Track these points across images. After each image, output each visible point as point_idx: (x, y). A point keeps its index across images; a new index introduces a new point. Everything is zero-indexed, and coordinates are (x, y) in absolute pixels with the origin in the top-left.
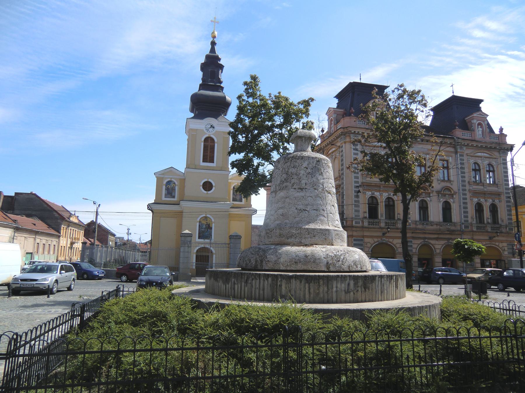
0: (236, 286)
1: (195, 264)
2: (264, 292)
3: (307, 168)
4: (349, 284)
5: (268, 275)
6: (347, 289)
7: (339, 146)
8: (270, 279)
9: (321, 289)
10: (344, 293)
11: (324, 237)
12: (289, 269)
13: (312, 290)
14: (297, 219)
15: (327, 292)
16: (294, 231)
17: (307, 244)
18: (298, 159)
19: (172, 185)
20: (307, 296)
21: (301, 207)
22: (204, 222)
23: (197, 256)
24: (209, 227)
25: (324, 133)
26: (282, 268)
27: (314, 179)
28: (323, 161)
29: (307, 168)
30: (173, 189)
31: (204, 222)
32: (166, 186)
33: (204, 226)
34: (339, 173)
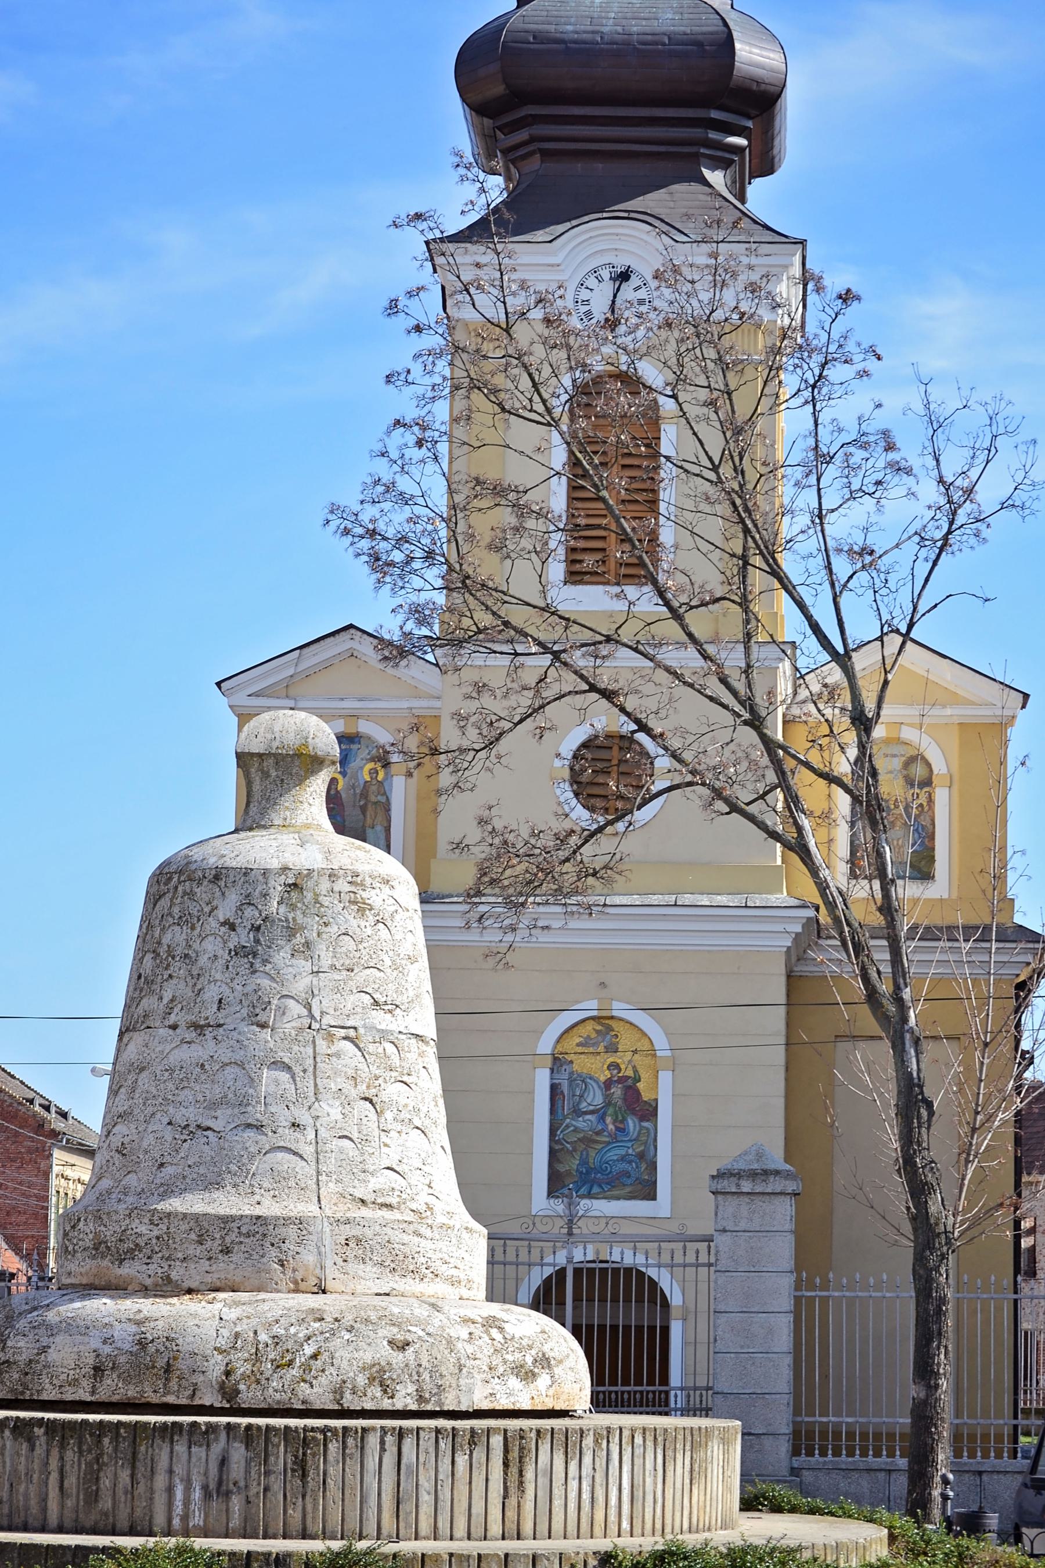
4: (223, 1462)
5: (64, 1424)
12: (68, 1397)
13: (71, 1481)
14: (169, 1170)
15: (131, 1492)
16: (143, 1229)
17: (194, 1285)
20: (53, 1506)
21: (191, 1114)
22: (594, 1066)
26: (50, 1394)
28: (325, 885)
29: (232, 927)
31: (594, 1066)
33: (595, 1098)
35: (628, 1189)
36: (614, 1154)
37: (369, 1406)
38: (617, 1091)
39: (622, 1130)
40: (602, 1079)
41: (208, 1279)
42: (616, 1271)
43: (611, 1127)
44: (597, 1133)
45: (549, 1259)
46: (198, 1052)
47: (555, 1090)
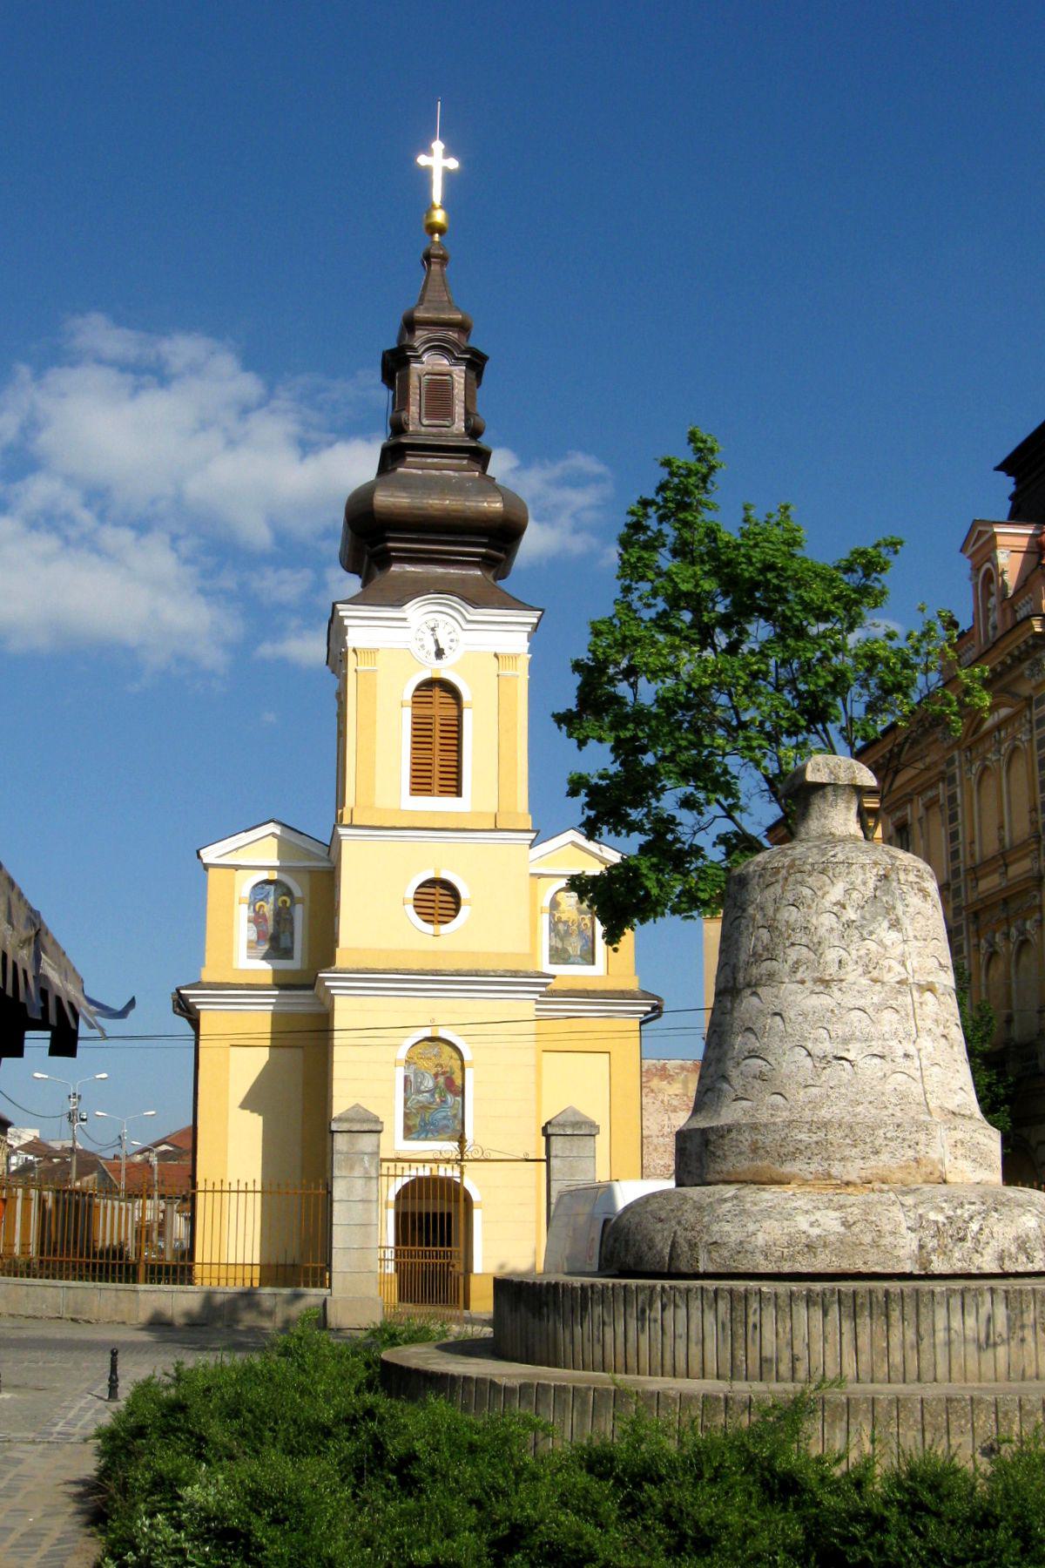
0: (609, 1332)
1: (390, 1254)
4: (990, 1319)
6: (983, 1336)
7: (1029, 699)
8: (723, 1306)
10: (972, 1348)
11: (911, 1153)
18: (810, 875)
23: (402, 1220)
24: (453, 1087)
32: (252, 904)
33: (429, 1083)
34: (1033, 823)
36: (439, 1115)
37: (1021, 1269)
38: (441, 1080)
41: (863, 1174)
46: (825, 1000)
47: (406, 1079)
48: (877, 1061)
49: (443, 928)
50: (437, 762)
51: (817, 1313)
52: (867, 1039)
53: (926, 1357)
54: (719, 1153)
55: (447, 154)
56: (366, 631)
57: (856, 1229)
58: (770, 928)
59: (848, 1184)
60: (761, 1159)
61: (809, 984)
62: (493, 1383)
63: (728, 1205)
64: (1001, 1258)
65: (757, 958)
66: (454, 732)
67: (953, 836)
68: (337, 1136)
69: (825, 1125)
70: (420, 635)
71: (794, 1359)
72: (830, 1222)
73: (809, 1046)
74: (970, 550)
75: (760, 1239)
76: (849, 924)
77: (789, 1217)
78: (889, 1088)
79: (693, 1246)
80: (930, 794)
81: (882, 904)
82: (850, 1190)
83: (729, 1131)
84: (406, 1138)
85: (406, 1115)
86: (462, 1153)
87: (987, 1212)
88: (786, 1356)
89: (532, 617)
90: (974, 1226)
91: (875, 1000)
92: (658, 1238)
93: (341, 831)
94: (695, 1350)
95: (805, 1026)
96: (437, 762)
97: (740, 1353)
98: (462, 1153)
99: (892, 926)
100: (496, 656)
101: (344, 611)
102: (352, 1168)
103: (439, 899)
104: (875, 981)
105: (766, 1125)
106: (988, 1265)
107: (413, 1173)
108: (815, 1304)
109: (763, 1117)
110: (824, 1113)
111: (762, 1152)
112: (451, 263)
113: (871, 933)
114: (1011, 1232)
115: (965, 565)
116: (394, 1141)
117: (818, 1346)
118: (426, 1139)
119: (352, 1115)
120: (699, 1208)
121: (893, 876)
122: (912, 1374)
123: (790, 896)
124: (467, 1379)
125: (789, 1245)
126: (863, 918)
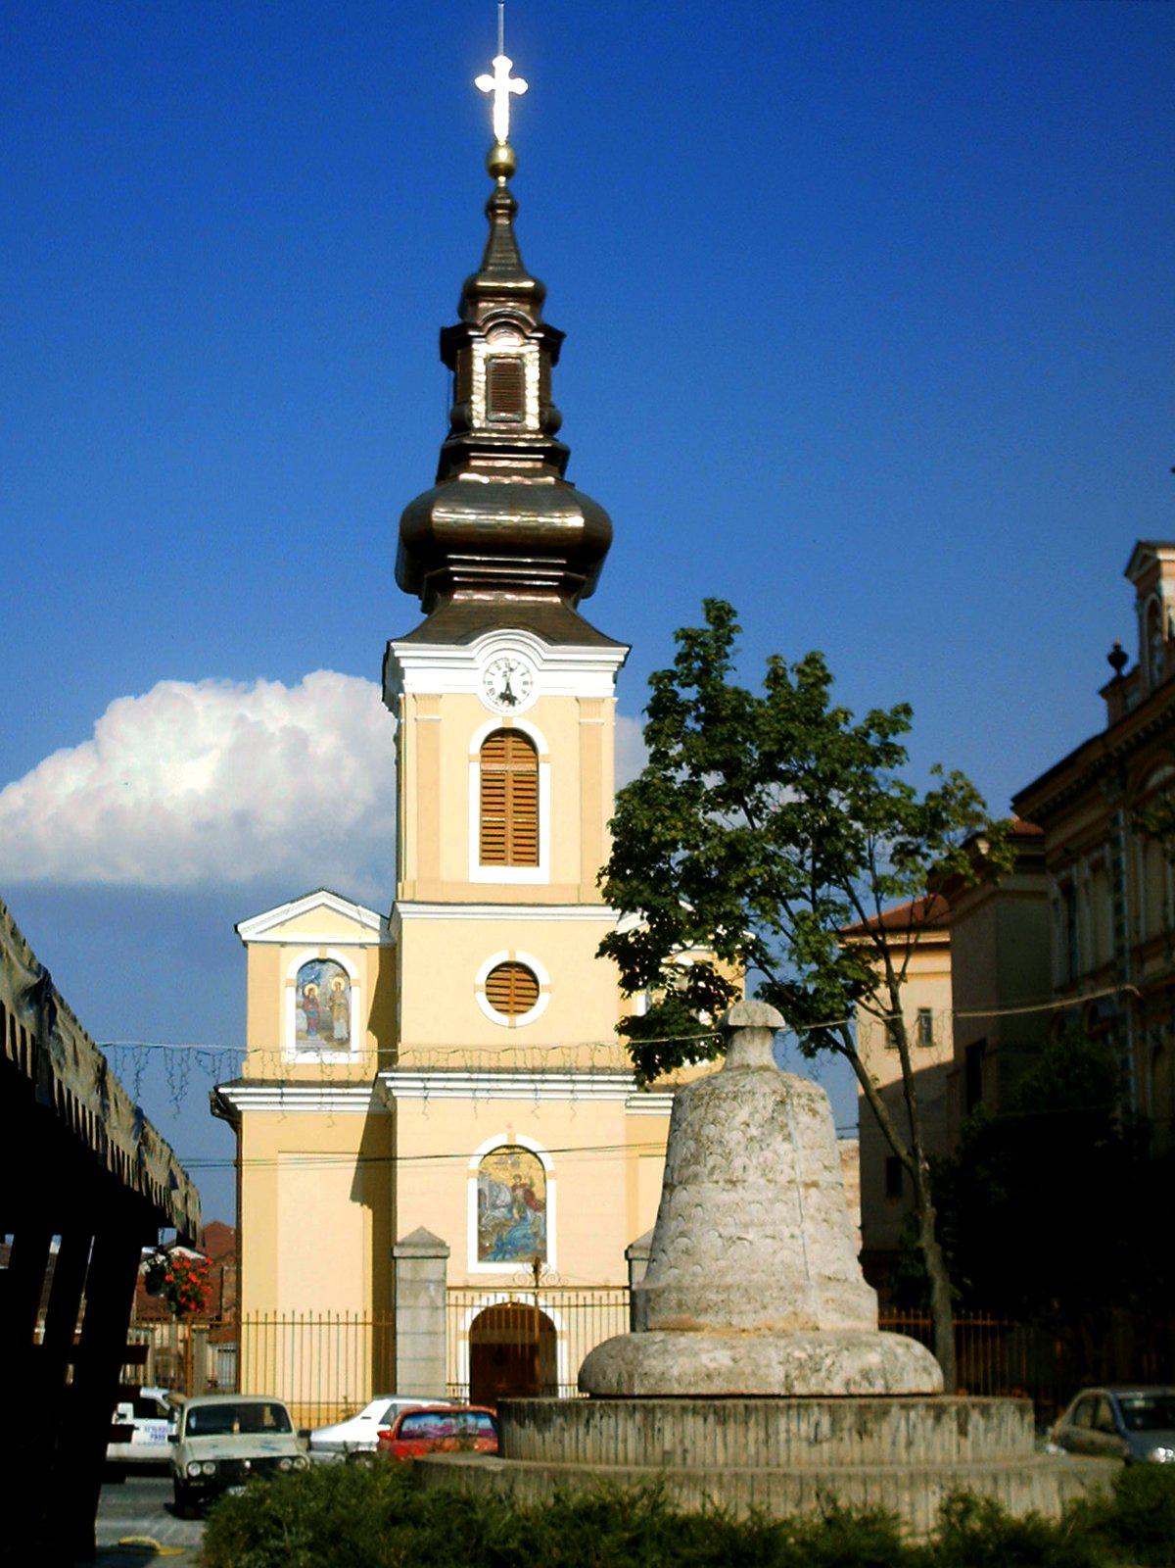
0: (566, 1434)
2: (626, 1449)
3: (748, 1125)
4: (817, 1425)
9: (751, 1436)
14: (722, 1263)
18: (725, 1100)
19: (331, 980)
23: (475, 1350)
24: (530, 1201)
25: (1126, 670)
27: (768, 1154)
30: (339, 1003)
31: (504, 1176)
32: (300, 987)
33: (506, 1197)
35: (526, 1257)
36: (518, 1234)
38: (520, 1193)
39: (523, 1218)
40: (511, 1184)
41: (755, 1324)
42: (523, 1312)
43: (516, 1216)
44: (507, 1220)
45: (477, 1303)
47: (480, 1192)
48: (769, 1241)
49: (520, 1019)
50: (510, 827)
51: (700, 1420)
52: (763, 1225)
53: (772, 1449)
54: (657, 1308)
55: (514, 74)
56: (427, 669)
57: (741, 1364)
58: (697, 1141)
59: (744, 1331)
60: (684, 1312)
61: (721, 1184)
62: (484, 1470)
63: (656, 1347)
64: (847, 1384)
65: (687, 1162)
66: (528, 787)
67: (1118, 908)
68: (399, 1262)
69: (728, 1288)
70: (489, 678)
71: (685, 1451)
72: (722, 1358)
73: (721, 1229)
74: (1136, 575)
75: (675, 1372)
76: (752, 1139)
77: (696, 1354)
78: (777, 1260)
79: (631, 1376)
80: (1096, 855)
81: (778, 1121)
82: (744, 1335)
83: (664, 1292)
84: (480, 1259)
85: (480, 1233)
86: (537, 1280)
87: (840, 1351)
88: (679, 1451)
89: (617, 655)
90: (828, 1361)
91: (770, 1195)
92: (609, 1371)
93: (401, 907)
94: (620, 1446)
95: (718, 1215)
96: (510, 827)
97: (650, 1448)
98: (537, 1280)
99: (784, 1140)
100: (577, 700)
101: (400, 650)
102: (416, 1297)
103: (513, 985)
104: (769, 1181)
105: (687, 1289)
106: (837, 1387)
107: (484, 1303)
108: (698, 1414)
109: (687, 1281)
110: (729, 1279)
111: (684, 1308)
112: (521, 213)
113: (768, 1145)
114: (858, 1364)
115: (1130, 591)
116: (467, 1264)
117: (700, 1443)
118: (503, 1260)
119: (416, 1239)
120: (637, 1348)
121: (788, 1101)
122: (762, 1461)
123: (710, 1117)
124: (469, 1467)
125: (695, 1374)
126: (763, 1134)
